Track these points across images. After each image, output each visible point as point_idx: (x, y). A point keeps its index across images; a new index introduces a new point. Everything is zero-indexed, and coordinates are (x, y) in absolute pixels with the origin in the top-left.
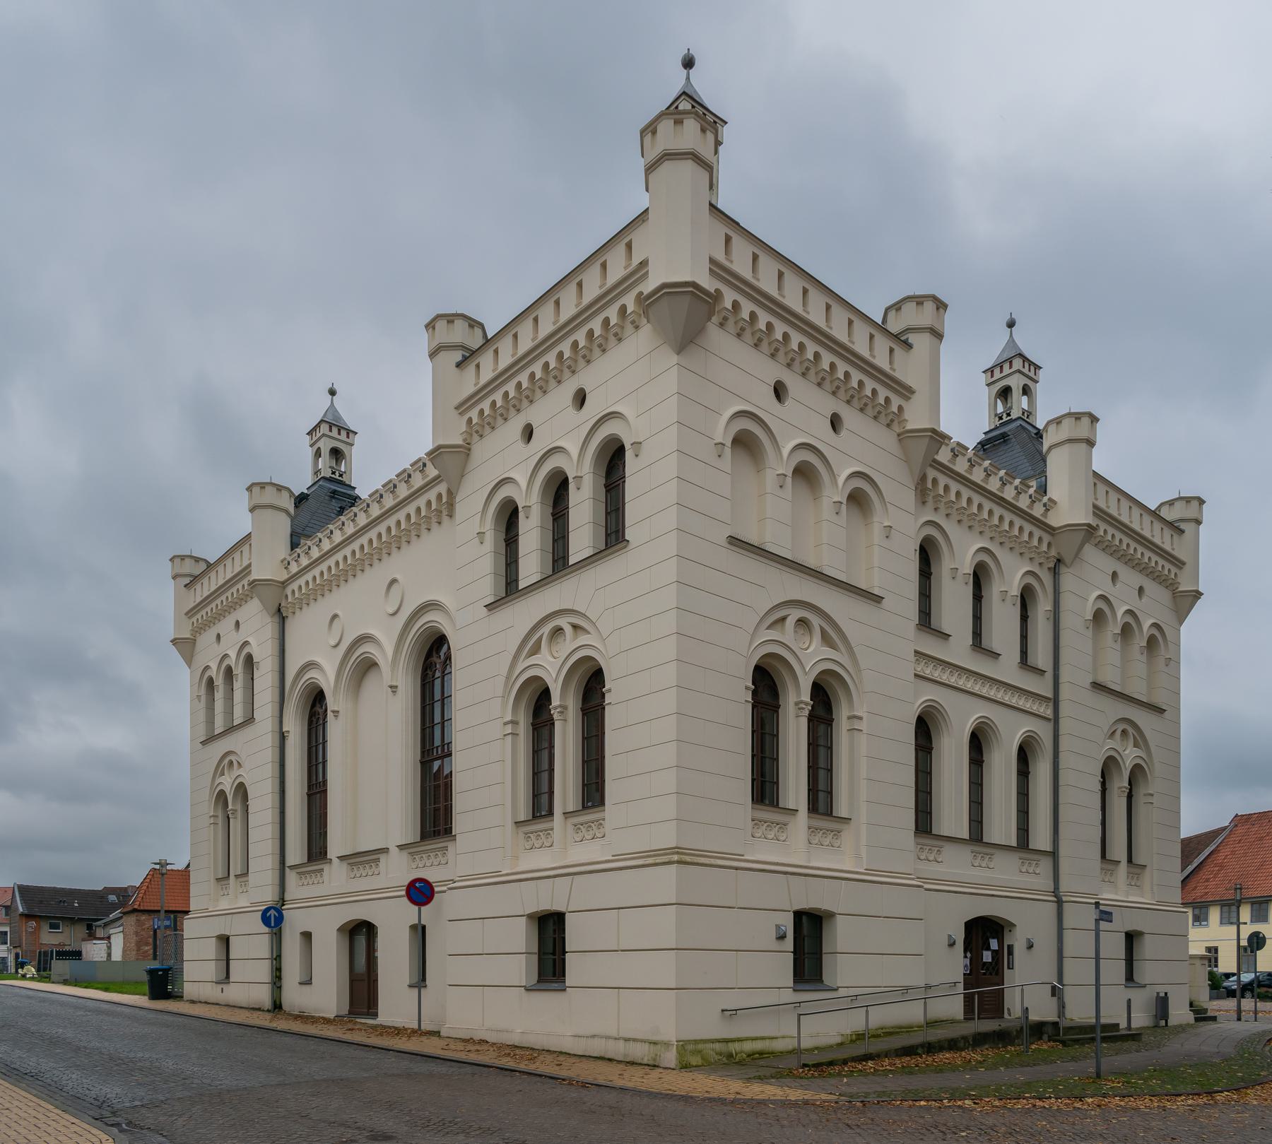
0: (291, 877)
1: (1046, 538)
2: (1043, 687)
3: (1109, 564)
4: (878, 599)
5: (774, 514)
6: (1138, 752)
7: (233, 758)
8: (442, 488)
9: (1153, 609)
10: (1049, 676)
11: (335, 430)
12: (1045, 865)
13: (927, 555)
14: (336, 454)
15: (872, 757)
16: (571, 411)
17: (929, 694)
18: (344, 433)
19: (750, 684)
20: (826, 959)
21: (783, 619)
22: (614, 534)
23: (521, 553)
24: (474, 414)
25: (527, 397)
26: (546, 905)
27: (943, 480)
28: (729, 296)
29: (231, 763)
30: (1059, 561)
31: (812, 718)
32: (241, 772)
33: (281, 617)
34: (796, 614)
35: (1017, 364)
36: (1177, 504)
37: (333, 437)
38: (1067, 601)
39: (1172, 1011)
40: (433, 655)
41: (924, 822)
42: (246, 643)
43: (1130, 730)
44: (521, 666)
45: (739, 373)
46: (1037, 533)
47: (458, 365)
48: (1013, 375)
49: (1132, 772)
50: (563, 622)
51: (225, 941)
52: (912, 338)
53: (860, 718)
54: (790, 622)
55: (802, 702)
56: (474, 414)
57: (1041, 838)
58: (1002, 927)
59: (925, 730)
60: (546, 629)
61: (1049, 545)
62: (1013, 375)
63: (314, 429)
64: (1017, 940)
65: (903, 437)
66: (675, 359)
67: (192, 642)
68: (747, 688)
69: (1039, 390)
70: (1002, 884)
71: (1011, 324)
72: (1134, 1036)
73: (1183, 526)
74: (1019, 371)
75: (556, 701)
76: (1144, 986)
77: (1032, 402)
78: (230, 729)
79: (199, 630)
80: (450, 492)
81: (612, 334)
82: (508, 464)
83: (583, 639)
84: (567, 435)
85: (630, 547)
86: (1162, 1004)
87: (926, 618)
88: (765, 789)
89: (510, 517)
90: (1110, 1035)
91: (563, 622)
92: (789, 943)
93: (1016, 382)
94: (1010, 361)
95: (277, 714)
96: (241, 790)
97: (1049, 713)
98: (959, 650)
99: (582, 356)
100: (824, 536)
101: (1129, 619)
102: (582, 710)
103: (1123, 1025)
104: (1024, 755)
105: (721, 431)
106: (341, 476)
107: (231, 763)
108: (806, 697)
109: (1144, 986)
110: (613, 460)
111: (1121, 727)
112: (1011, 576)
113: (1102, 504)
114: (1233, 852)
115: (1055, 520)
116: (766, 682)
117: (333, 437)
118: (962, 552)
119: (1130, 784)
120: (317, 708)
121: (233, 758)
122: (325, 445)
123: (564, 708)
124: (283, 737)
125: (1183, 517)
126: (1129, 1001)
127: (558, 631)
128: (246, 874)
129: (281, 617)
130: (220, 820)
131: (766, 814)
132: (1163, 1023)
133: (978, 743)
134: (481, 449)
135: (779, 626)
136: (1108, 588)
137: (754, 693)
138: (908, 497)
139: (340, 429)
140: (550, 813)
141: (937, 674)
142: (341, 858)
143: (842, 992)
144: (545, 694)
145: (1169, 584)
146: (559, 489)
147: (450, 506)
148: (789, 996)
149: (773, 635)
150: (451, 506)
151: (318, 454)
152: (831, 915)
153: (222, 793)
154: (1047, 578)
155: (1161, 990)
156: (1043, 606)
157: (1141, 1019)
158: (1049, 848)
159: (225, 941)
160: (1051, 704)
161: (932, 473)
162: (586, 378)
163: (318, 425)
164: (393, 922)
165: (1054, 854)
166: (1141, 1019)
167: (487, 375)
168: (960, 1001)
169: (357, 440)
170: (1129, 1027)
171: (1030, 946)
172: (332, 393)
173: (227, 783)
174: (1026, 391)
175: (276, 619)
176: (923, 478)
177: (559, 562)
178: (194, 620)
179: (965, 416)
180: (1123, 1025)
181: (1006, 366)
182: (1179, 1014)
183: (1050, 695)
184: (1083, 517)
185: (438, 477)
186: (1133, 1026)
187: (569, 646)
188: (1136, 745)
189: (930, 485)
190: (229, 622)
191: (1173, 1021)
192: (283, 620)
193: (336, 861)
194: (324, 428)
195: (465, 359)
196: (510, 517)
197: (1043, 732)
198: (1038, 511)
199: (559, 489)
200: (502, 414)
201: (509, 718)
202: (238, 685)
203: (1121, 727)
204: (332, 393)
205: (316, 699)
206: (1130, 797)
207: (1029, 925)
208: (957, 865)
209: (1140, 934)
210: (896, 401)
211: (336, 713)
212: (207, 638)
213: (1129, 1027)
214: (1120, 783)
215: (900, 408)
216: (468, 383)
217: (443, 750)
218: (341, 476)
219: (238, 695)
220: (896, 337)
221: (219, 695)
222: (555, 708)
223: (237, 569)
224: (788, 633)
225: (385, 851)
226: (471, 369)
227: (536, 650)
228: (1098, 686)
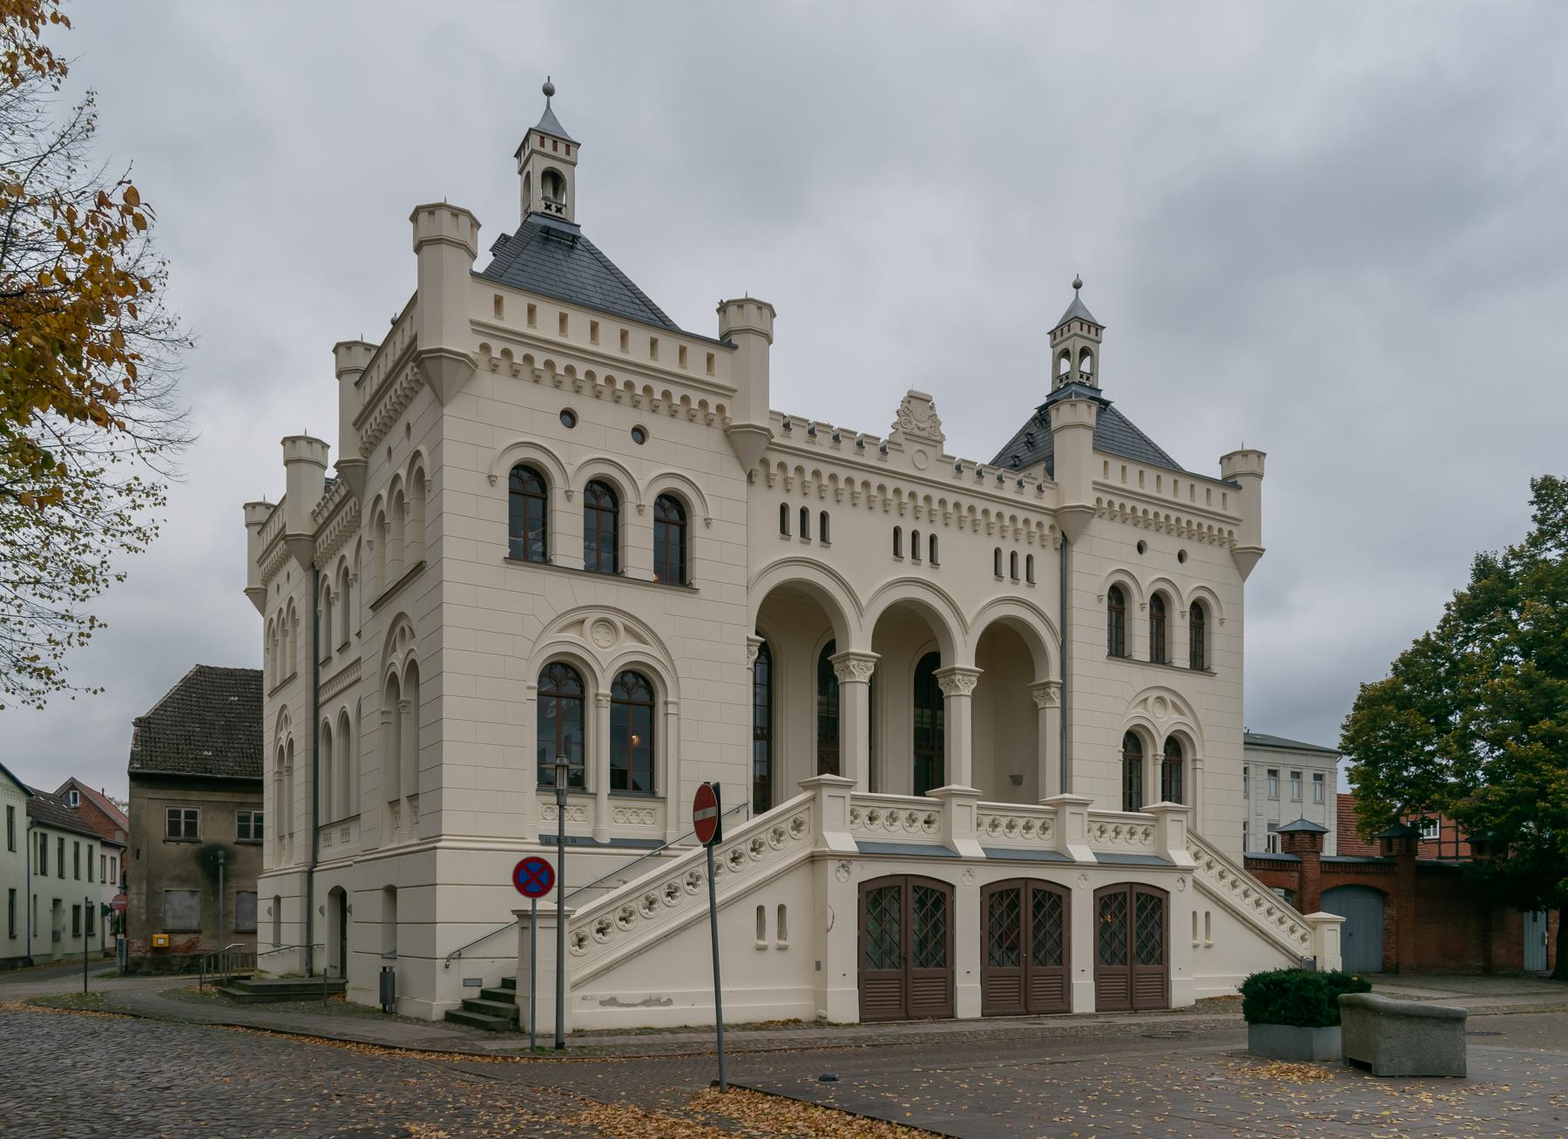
7: (403, 623)
11: (549, 143)
14: (554, 179)
18: (561, 147)
20: (660, 710)
36: (258, 508)
43: (1167, 696)
47: (357, 384)
51: (391, 891)
54: (588, 624)
60: (398, 630)
63: (522, 147)
65: (730, 433)
71: (1077, 286)
77: (1094, 365)
79: (267, 579)
96: (413, 667)
106: (559, 210)
107: (403, 630)
122: (538, 166)
136: (1173, 570)
153: (394, 676)
159: (391, 891)
163: (526, 139)
169: (582, 155)
172: (549, 91)
173: (398, 660)
175: (311, 572)
178: (363, 432)
190: (399, 428)
192: (317, 573)
204: (549, 91)
214: (1155, 755)
215: (720, 408)
218: (559, 210)
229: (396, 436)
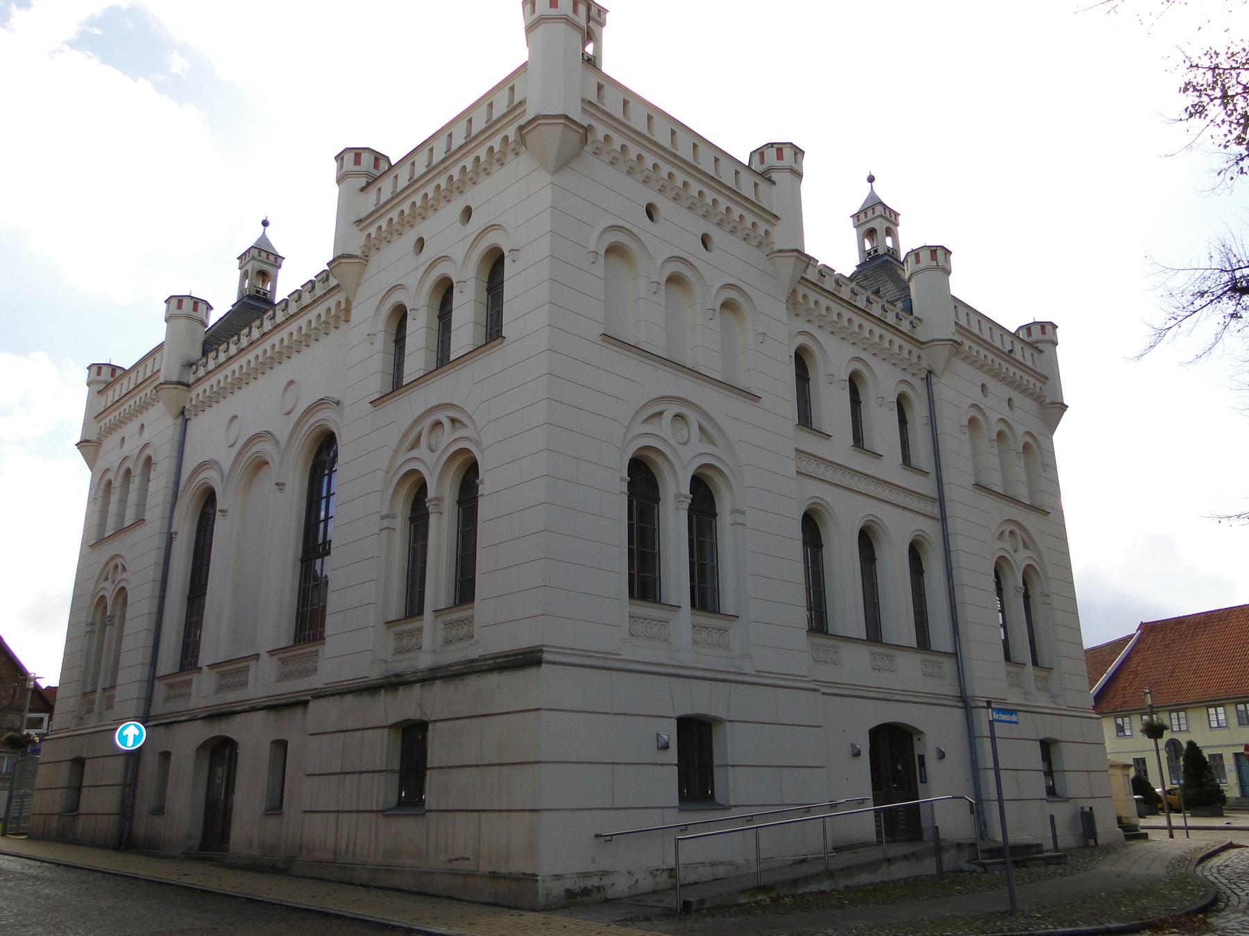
0: (160, 688)
1: (916, 352)
2: (926, 486)
3: (979, 377)
4: (756, 398)
5: (646, 318)
6: (1028, 553)
8: (341, 296)
9: (1024, 417)
10: (933, 476)
12: (948, 666)
13: (801, 361)
14: (263, 275)
15: (759, 551)
16: (458, 225)
17: (813, 491)
18: (272, 258)
19: (625, 474)
20: (718, 774)
21: (661, 413)
22: (493, 330)
23: (407, 352)
24: (373, 230)
25: (419, 214)
26: (412, 713)
27: (813, 296)
28: (601, 131)
29: (116, 566)
30: (930, 372)
31: (692, 511)
32: (125, 576)
33: (183, 416)
34: (671, 410)
35: (879, 210)
37: (261, 262)
38: (943, 410)
39: (1100, 829)
40: (324, 451)
41: (818, 623)
42: (146, 445)
43: (1017, 531)
44: (401, 460)
45: (614, 196)
46: (907, 347)
47: (363, 189)
48: (875, 219)
49: (1025, 572)
50: (442, 416)
52: (775, 176)
53: (743, 513)
54: (668, 416)
55: (681, 495)
56: (373, 230)
57: (941, 637)
58: (911, 736)
59: (812, 526)
60: (112, 565)
61: (919, 357)
62: (875, 219)
64: (928, 747)
66: (547, 178)
67: (99, 443)
68: (622, 479)
69: (901, 231)
70: (905, 686)
72: (1059, 858)
73: (1041, 346)
74: (881, 216)
75: (431, 493)
76: (1068, 800)
77: (896, 241)
78: (120, 531)
80: (348, 301)
81: (497, 159)
82: (400, 272)
83: (461, 433)
84: (454, 246)
85: (506, 342)
86: (1087, 819)
87: (805, 418)
88: (644, 582)
89: (400, 316)
90: (1024, 855)
91: (442, 416)
92: (672, 755)
93: (880, 225)
94: (872, 207)
95: (168, 515)
97: (936, 511)
98: (840, 447)
99: (471, 178)
100: (701, 342)
101: (1002, 427)
102: (459, 502)
103: (1049, 844)
104: (915, 553)
105: (595, 241)
107: (116, 566)
108: (686, 490)
109: (1068, 800)
110: (495, 263)
111: (1009, 528)
112: (883, 385)
113: (963, 323)
114: (1144, 660)
115: (921, 334)
116: (642, 477)
117: (261, 262)
118: (834, 362)
119: (1025, 583)
120: (209, 509)
121: (118, 561)
123: (439, 499)
124: (170, 538)
125: (1040, 338)
126: (1052, 817)
127: (438, 424)
128: (113, 687)
129: (183, 416)
130: (97, 628)
131: (645, 609)
132: (1092, 842)
133: (867, 540)
134: (376, 260)
135: (656, 420)
137: (630, 485)
138: (780, 309)
139: (268, 254)
140: (421, 612)
141: (820, 471)
142: (212, 666)
143: (734, 813)
144: (422, 488)
145: (1039, 399)
146: (445, 291)
147: (344, 313)
148: (675, 818)
149: (648, 428)
150: (348, 310)
151: (245, 276)
152: (720, 721)
153: (103, 597)
154: (921, 387)
155: (1086, 805)
156: (917, 415)
157: (1067, 840)
158: (950, 649)
160: (937, 504)
161: (802, 290)
162: (472, 197)
164: (254, 735)
165: (956, 655)
166: (1067, 840)
167: (386, 195)
168: (870, 820)
170: (1056, 849)
171: (942, 755)
174: (889, 232)
175: (180, 421)
176: (794, 292)
177: (443, 358)
178: (102, 424)
179: (834, 247)
180: (1049, 844)
181: (870, 212)
182: (1107, 828)
183: (935, 495)
184: (949, 332)
185: (338, 286)
186: (1061, 845)
187: (448, 440)
188: (1026, 546)
189: (800, 300)
190: (133, 426)
191: (1103, 838)
193: (205, 669)
194: (256, 252)
195: (368, 184)
196: (400, 316)
197: (931, 530)
198: (905, 326)
199: (445, 291)
200: (395, 231)
201: (385, 512)
202: (134, 486)
203: (1009, 528)
204: (265, 223)
205: (208, 499)
206: (1026, 597)
207: (938, 731)
208: (856, 664)
209: (1056, 742)
210: (762, 227)
211: (223, 511)
212: (112, 441)
213: (1056, 849)
215: (767, 232)
216: (368, 203)
217: (324, 549)
219: (133, 497)
220: (761, 175)
221: (115, 497)
222: (431, 501)
223: (148, 374)
224: (665, 427)
225: (257, 657)
226: (373, 192)
227: (416, 444)
228: (980, 487)
229: (131, 429)
